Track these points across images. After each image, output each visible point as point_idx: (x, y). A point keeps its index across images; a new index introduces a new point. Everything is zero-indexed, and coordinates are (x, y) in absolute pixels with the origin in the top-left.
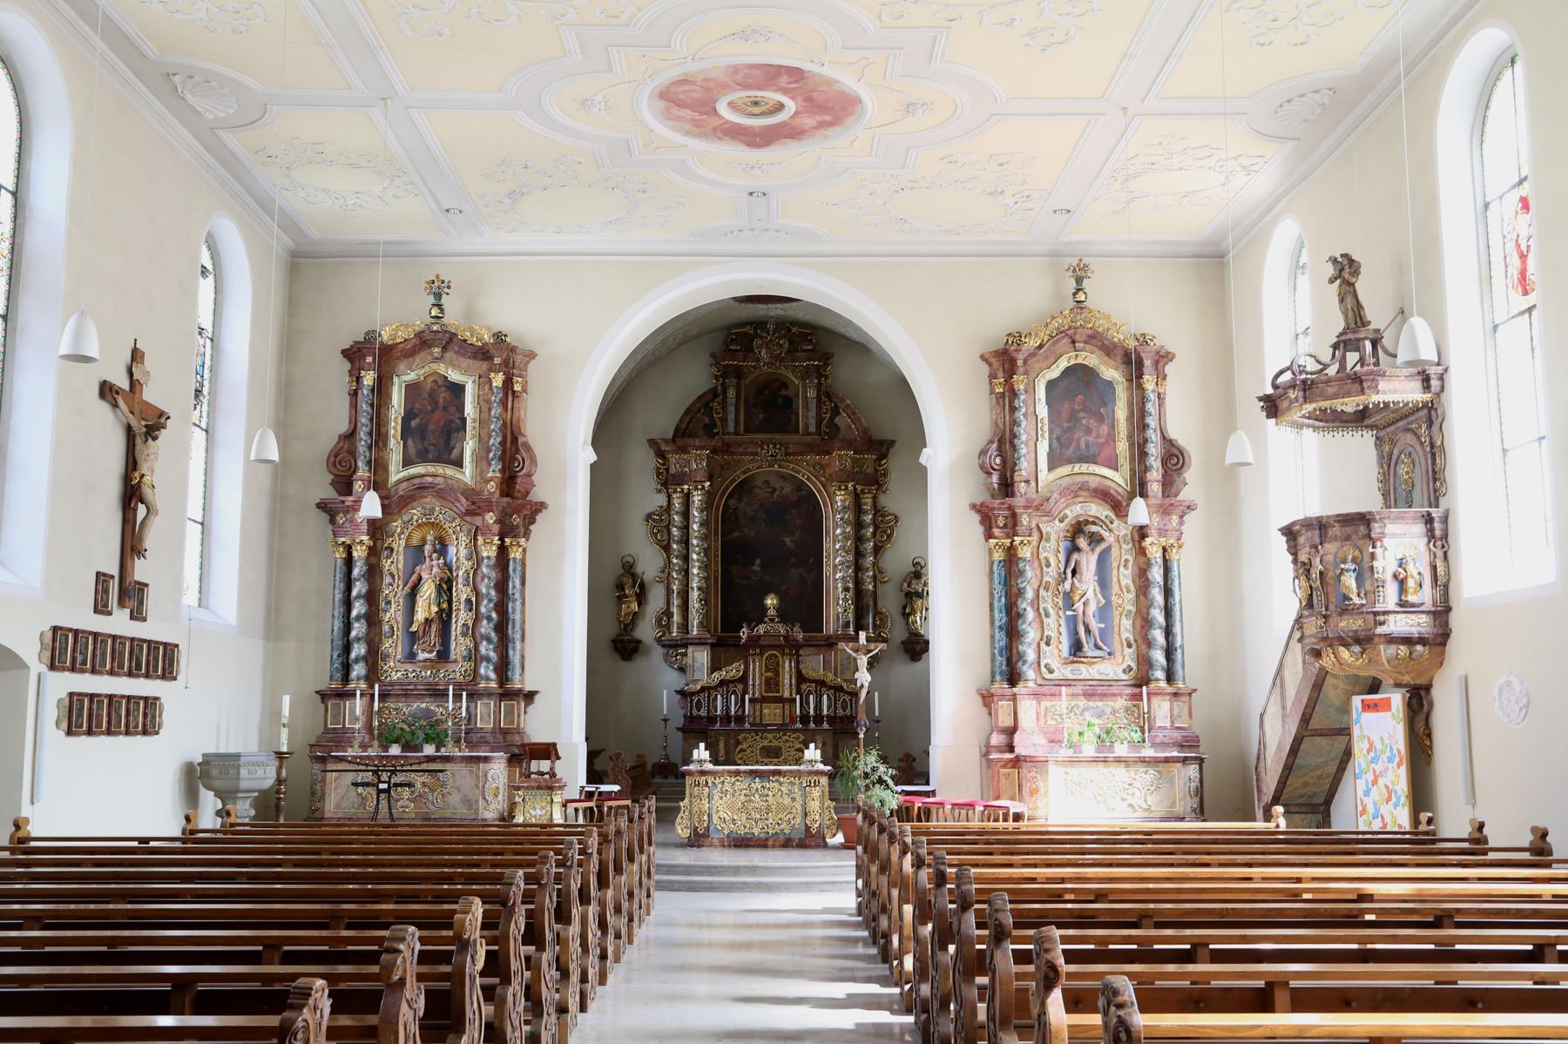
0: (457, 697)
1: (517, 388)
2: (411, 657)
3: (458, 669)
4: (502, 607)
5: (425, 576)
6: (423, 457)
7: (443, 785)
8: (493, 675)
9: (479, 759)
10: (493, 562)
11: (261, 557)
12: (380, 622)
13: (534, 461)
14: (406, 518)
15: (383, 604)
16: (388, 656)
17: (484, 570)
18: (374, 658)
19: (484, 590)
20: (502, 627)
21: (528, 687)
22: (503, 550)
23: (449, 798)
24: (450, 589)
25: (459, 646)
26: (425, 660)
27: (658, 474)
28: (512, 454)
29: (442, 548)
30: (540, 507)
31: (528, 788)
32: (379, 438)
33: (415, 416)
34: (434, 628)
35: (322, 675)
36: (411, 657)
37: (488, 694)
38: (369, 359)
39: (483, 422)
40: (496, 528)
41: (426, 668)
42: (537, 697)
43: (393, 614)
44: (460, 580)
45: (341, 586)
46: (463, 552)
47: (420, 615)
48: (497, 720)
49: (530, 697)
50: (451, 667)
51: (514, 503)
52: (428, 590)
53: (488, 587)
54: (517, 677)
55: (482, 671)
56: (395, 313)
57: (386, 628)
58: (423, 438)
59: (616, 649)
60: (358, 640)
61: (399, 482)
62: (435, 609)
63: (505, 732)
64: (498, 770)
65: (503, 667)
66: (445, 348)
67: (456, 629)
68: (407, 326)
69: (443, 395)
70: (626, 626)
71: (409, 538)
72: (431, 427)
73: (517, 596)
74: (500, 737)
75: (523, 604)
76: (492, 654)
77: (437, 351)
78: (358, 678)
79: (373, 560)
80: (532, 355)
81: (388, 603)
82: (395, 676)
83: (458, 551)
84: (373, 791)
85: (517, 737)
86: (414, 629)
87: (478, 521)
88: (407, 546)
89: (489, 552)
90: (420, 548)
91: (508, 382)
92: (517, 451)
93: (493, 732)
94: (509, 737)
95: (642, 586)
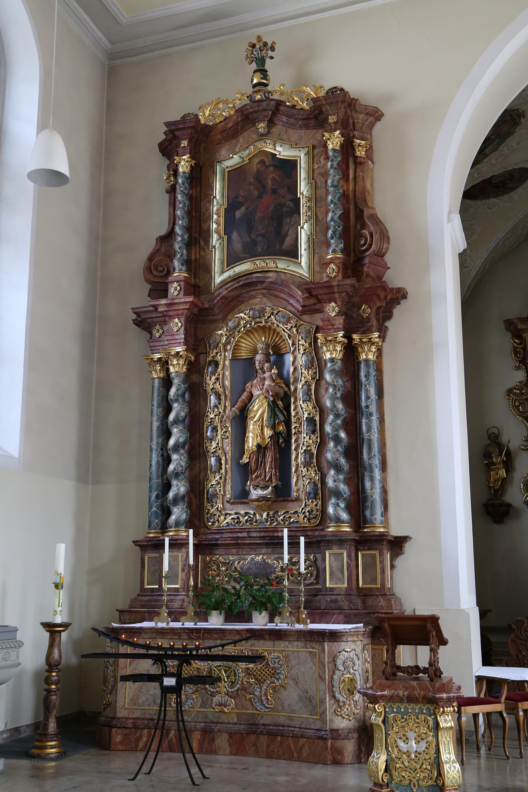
0: (294, 545)
1: (360, 153)
2: (242, 496)
3: (301, 510)
4: (353, 424)
6: (250, 252)
7: (275, 674)
8: (344, 516)
9: (322, 635)
10: (338, 365)
11: (69, 380)
13: (385, 237)
16: (215, 495)
17: (328, 377)
18: (198, 499)
19: (328, 404)
20: (354, 451)
21: (395, 531)
22: (351, 351)
23: (284, 694)
24: (287, 408)
25: (301, 480)
27: (516, 353)
28: (359, 235)
29: (276, 355)
30: (399, 295)
31: (391, 699)
32: (198, 235)
33: (241, 204)
35: (139, 527)
36: (242, 496)
37: (339, 540)
38: (184, 143)
39: (317, 199)
40: (340, 322)
42: (408, 547)
43: (219, 443)
44: (300, 394)
45: (157, 411)
46: (302, 360)
48: (353, 578)
49: (397, 544)
50: (293, 507)
51: (364, 294)
52: (259, 409)
53: (333, 398)
54: (378, 517)
55: (331, 510)
56: (213, 90)
57: (213, 461)
58: (250, 229)
59: (488, 513)
60: (176, 475)
61: (224, 283)
62: (268, 432)
63: (365, 594)
64: (354, 653)
65: (358, 505)
66: (271, 123)
67: (297, 458)
68: (226, 102)
69: (271, 176)
70: (496, 491)
72: (259, 215)
73: (373, 408)
74: (358, 602)
75: (382, 420)
76: (343, 487)
77: (262, 126)
78: (177, 524)
79: (195, 378)
80: (376, 115)
81: (215, 429)
82: (225, 521)
83: (296, 361)
84: (154, 688)
85: (382, 602)
86: (245, 460)
87: (318, 319)
88: (234, 359)
89: (333, 353)
90: (251, 361)
91: (347, 147)
92: (364, 226)
93: (348, 593)
94: (370, 601)
95: (509, 454)
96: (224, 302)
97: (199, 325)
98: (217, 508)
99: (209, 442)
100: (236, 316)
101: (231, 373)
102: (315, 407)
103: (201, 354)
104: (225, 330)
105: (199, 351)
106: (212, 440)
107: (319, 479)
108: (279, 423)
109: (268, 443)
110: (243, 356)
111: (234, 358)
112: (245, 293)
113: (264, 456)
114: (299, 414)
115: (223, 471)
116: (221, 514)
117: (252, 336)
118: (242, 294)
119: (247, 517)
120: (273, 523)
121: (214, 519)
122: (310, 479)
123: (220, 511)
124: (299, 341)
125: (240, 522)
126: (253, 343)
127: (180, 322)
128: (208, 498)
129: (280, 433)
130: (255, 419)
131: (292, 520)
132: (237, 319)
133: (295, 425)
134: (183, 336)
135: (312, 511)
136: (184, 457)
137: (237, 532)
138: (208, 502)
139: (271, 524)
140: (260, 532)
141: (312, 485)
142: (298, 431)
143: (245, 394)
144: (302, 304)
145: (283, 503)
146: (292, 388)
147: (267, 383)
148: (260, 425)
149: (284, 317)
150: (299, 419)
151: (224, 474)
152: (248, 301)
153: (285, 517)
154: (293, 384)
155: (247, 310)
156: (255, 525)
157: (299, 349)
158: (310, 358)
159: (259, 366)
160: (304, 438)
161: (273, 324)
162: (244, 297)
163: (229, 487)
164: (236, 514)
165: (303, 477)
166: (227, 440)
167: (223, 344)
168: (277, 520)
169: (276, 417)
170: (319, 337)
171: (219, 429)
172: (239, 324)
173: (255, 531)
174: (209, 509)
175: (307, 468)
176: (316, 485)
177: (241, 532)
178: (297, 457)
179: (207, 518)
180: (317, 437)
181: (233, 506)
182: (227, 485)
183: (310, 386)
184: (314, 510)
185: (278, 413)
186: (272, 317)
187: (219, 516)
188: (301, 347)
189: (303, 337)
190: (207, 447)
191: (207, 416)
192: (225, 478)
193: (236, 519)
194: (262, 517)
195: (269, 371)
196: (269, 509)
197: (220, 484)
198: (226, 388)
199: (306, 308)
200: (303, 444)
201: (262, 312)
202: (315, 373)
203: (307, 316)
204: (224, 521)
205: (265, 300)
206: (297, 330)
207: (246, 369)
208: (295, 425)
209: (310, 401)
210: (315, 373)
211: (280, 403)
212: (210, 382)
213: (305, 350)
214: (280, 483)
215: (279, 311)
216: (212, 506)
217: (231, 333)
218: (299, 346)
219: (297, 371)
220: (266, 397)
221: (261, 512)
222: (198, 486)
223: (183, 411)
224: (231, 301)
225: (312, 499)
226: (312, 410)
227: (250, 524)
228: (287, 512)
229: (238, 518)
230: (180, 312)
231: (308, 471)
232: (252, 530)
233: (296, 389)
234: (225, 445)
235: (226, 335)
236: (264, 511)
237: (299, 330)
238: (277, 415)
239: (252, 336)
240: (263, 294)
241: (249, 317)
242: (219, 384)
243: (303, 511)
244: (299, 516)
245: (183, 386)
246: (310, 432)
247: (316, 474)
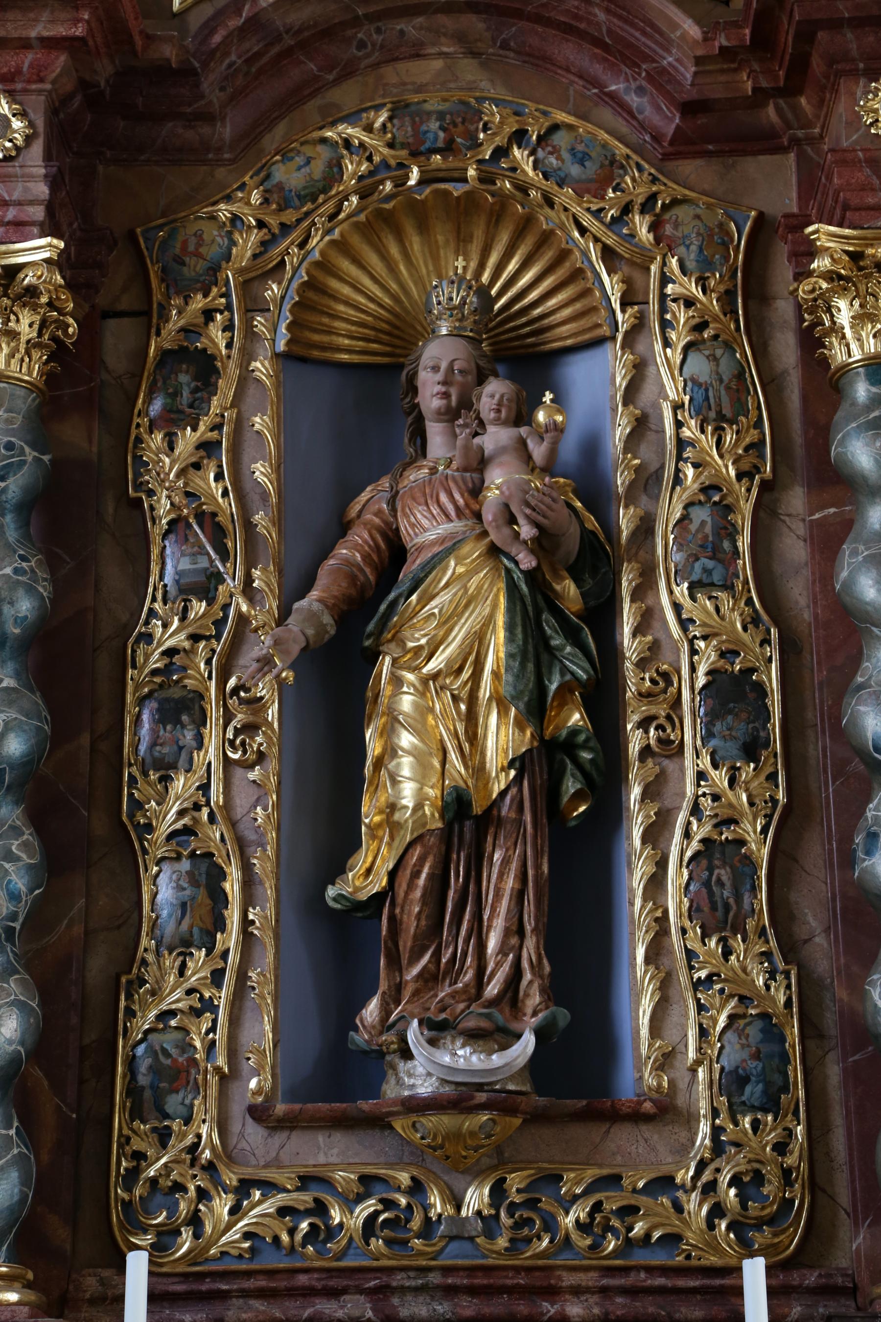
2: (338, 1082)
5: (427, 528)
12: (124, 847)
14: (290, 175)
15: (143, 730)
16: (178, 1074)
24: (602, 614)
26: (461, 1097)
34: (503, 872)
36: (338, 1082)
41: (455, 1161)
43: (214, 784)
47: (407, 783)
50: (638, 1154)
57: (164, 889)
62: (501, 738)
67: (653, 883)
71: (313, 300)
79: (78, 435)
86: (366, 873)
96: (258, 55)
97: (100, 168)
98: (193, 1149)
99: (153, 776)
100: (316, 135)
101: (285, 425)
102: (756, 620)
103: (107, 315)
104: (255, 198)
105: (102, 300)
106: (174, 766)
107: (788, 1004)
108: (565, 689)
109: (503, 794)
110: (340, 349)
111: (298, 350)
112: (371, 18)
113: (477, 862)
114: (667, 653)
115: (230, 938)
116: (217, 1182)
117: (394, 250)
118: (356, 22)
119: (370, 1206)
120: (528, 1241)
121: (173, 1210)
122: (742, 999)
123: (210, 1168)
124: (665, 280)
125: (332, 1232)
126: (394, 286)
127: (22, 114)
128: (133, 1090)
129: (568, 745)
130: (433, 665)
131: (639, 1228)
132: (324, 153)
133: (645, 709)
134: (42, 190)
135: (759, 1178)
136: (25, 845)
137: (309, 1293)
138: (136, 1113)
139: (517, 1244)
140: (450, 1291)
141: (754, 1032)
142: (664, 742)
143: (359, 536)
144: (689, 93)
145: (577, 1131)
146: (625, 521)
147: (498, 479)
148: (464, 694)
149: (582, 159)
150: (666, 676)
151: (233, 958)
152: (376, 65)
153: (597, 1207)
154: (631, 497)
155: (378, 108)
156: (421, 1254)
157: (665, 325)
158: (726, 369)
159: (446, 395)
160: (701, 776)
161: (523, 188)
162: (362, 45)
163: (262, 1031)
164: (305, 1181)
165: (697, 985)
166: (255, 774)
167: (240, 271)
168: (550, 1225)
169: (545, 657)
170: (823, 242)
171: (214, 712)
172: (335, 169)
173: (418, 1290)
174: (139, 1156)
175: (723, 940)
176: (772, 1030)
177: (334, 1293)
178: (656, 884)
179: (127, 1205)
180: (772, 777)
181: (279, 1138)
182: (248, 1018)
183: (729, 509)
184: (771, 1172)
185: (556, 642)
186: (516, 152)
187: (203, 1195)
188: (682, 315)
189: (691, 265)
190: (137, 805)
191: (148, 637)
192: (242, 976)
193: (308, 1213)
194: (458, 1208)
195: (505, 423)
196: (494, 1163)
197: (214, 1009)
198: (254, 498)
199: (702, 120)
200: (696, 810)
201: (463, 122)
202: (757, 446)
203: (699, 162)
204: (229, 1227)
205: (469, 71)
206: (654, 227)
207: (363, 403)
208: (645, 709)
209: (728, 587)
210: (757, 446)
211: (569, 589)
212: (166, 461)
213: (700, 327)
214: (564, 1016)
215: (555, 128)
216: (164, 1137)
217: (289, 217)
218: (663, 310)
219: (651, 436)
220: (494, 551)
221: (456, 1180)
222: (74, 1020)
223: (30, 590)
224: (288, 53)
225: (753, 1109)
226: (746, 637)
227: (388, 1242)
228: (614, 1180)
229: (320, 1209)
230: (28, 59)
231: (727, 953)
232: (398, 1280)
233: (645, 529)
234: (241, 803)
235: (261, 224)
236: (476, 1174)
237: (668, 229)
238: (551, 651)
239: (394, 250)
240: (460, 38)
241: (391, 145)
242: (219, 477)
243: (706, 1177)
244: (679, 1208)
245: (30, 454)
246: (732, 748)
247: (772, 974)
